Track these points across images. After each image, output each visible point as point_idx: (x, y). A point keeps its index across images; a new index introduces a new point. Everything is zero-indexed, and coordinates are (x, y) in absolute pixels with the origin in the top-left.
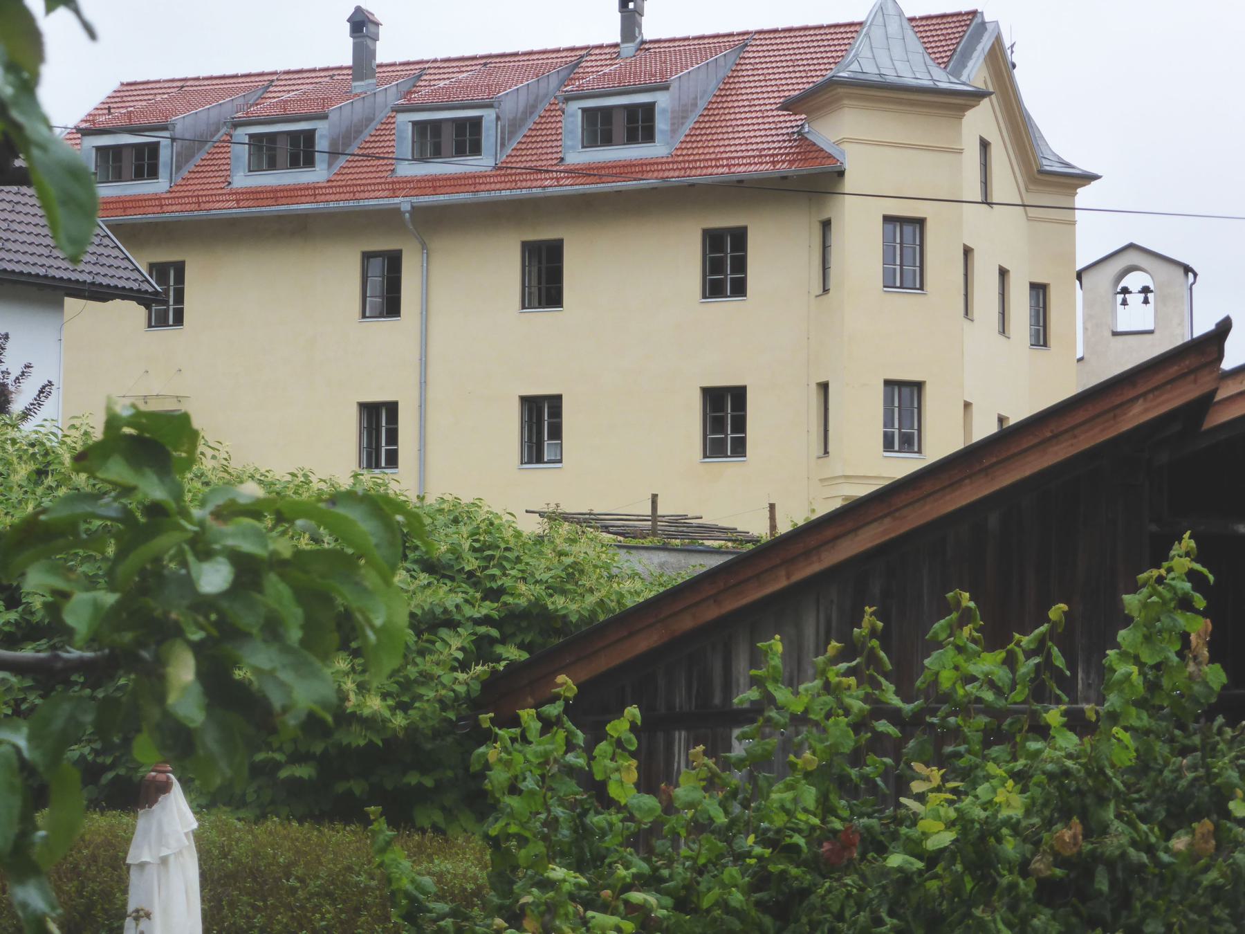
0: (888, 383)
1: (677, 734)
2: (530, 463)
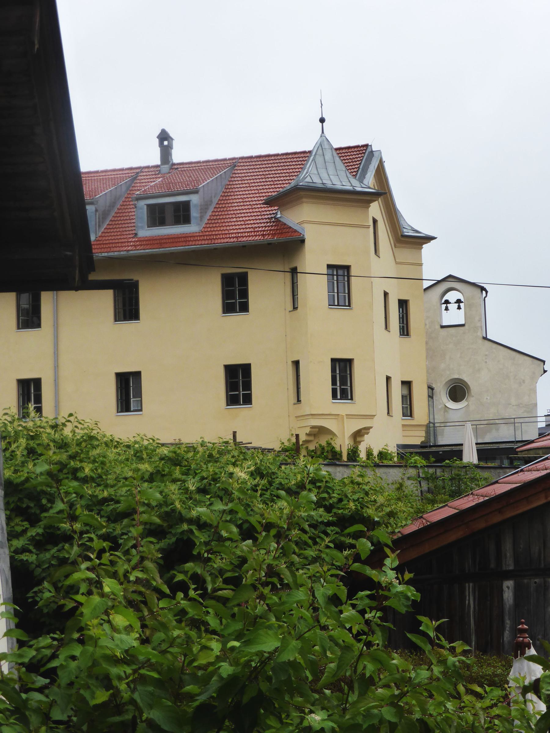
0: (334, 361)
1: (467, 585)
2: (122, 412)
